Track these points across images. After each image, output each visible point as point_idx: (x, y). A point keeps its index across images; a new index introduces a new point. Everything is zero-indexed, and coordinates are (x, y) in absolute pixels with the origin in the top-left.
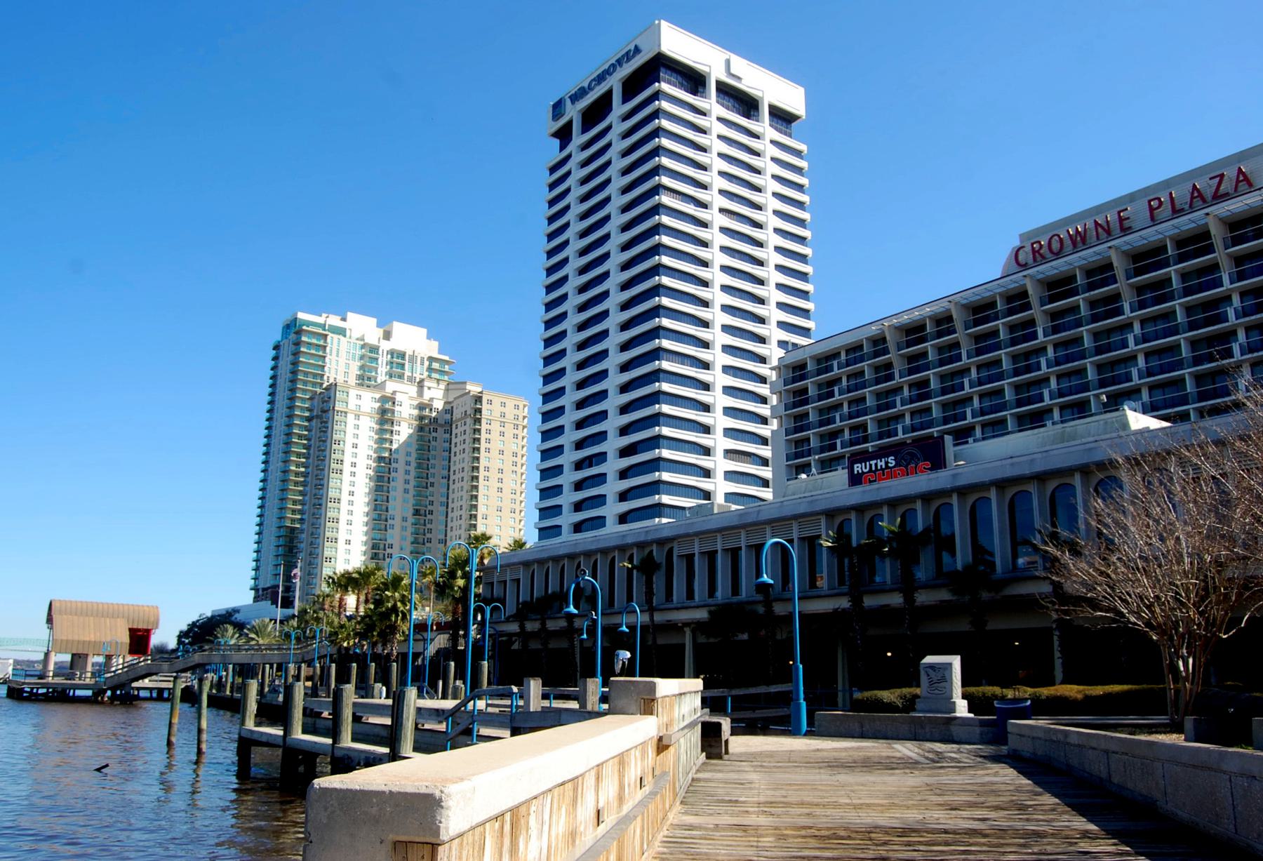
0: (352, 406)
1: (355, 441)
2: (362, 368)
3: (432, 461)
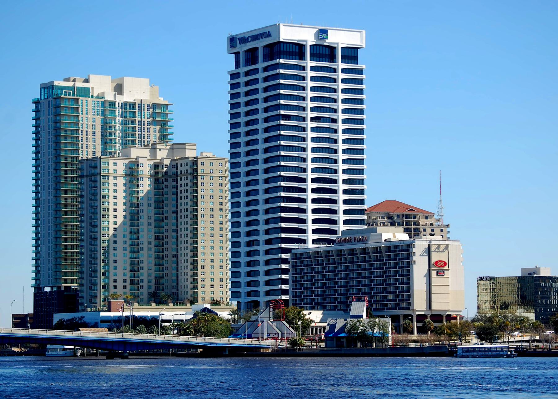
0: (111, 171)
1: (115, 194)
3: (165, 202)
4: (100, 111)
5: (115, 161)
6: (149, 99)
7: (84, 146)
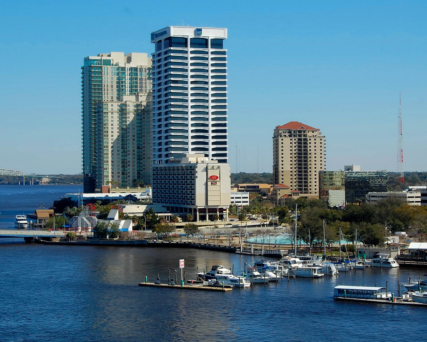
2: (118, 78)
4: (116, 73)
5: (112, 104)
7: (106, 94)
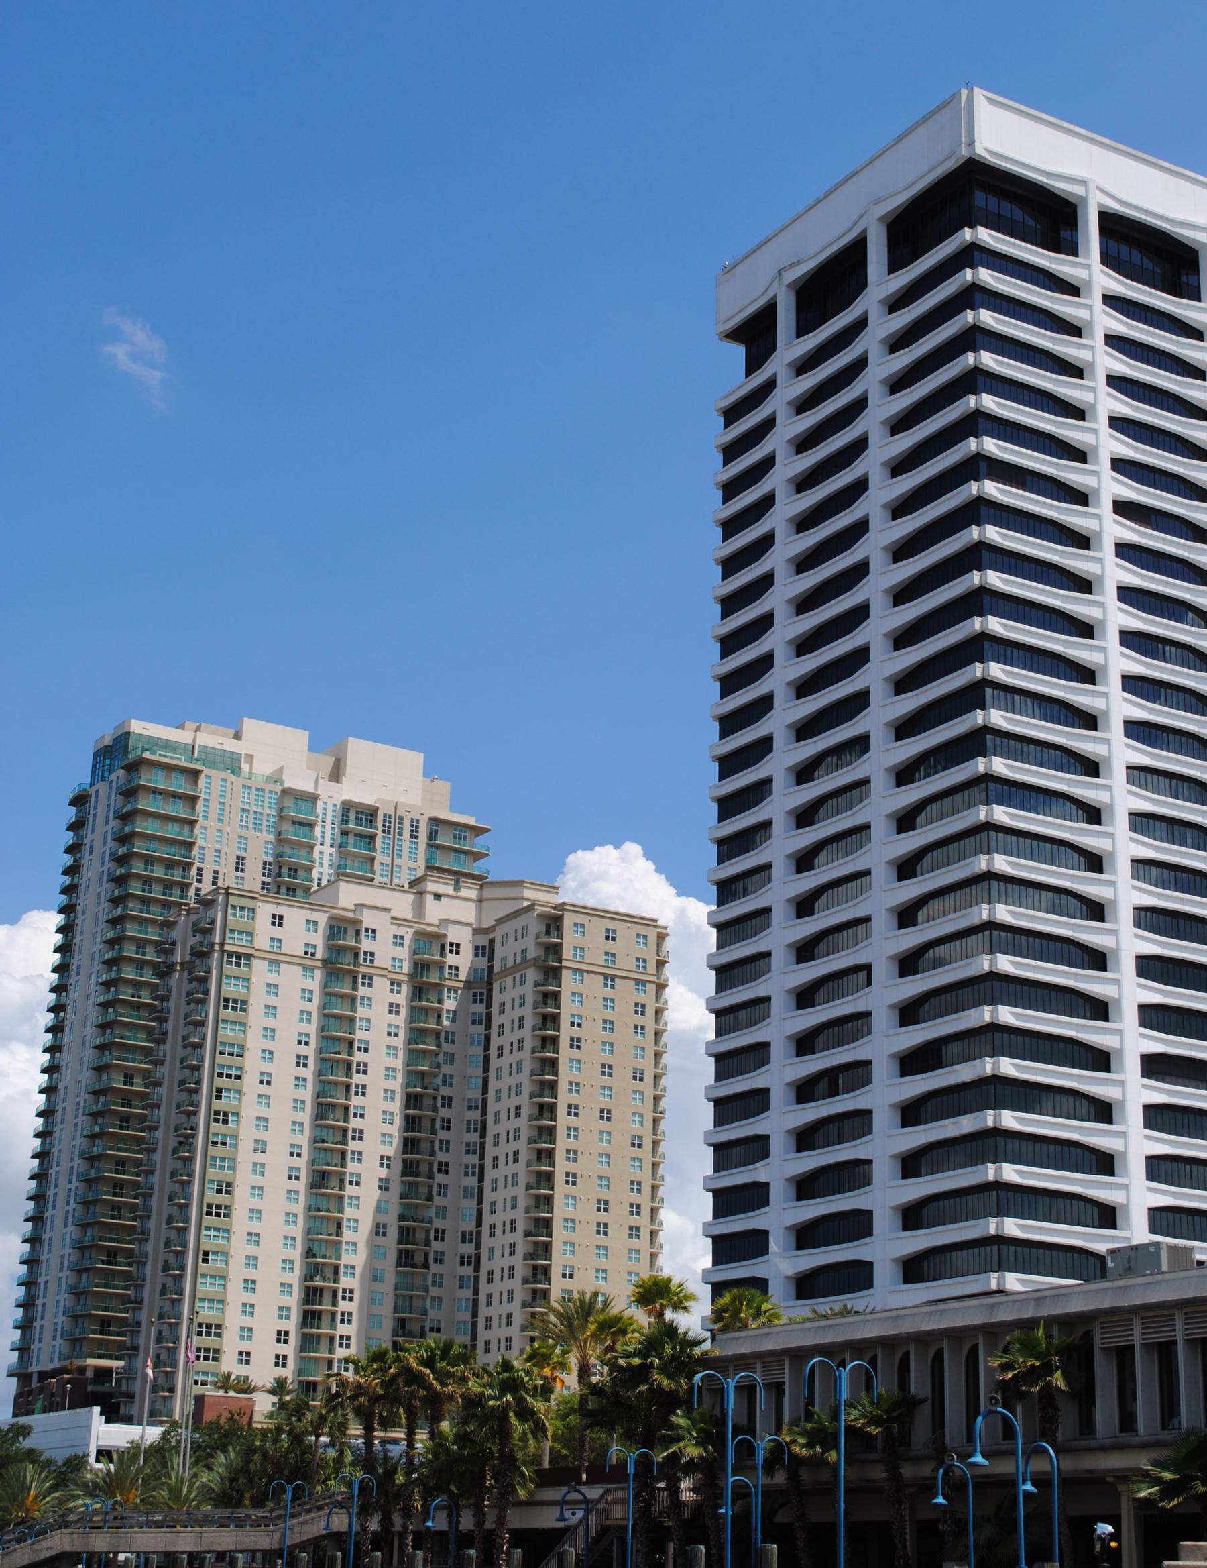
6: (419, 804)
